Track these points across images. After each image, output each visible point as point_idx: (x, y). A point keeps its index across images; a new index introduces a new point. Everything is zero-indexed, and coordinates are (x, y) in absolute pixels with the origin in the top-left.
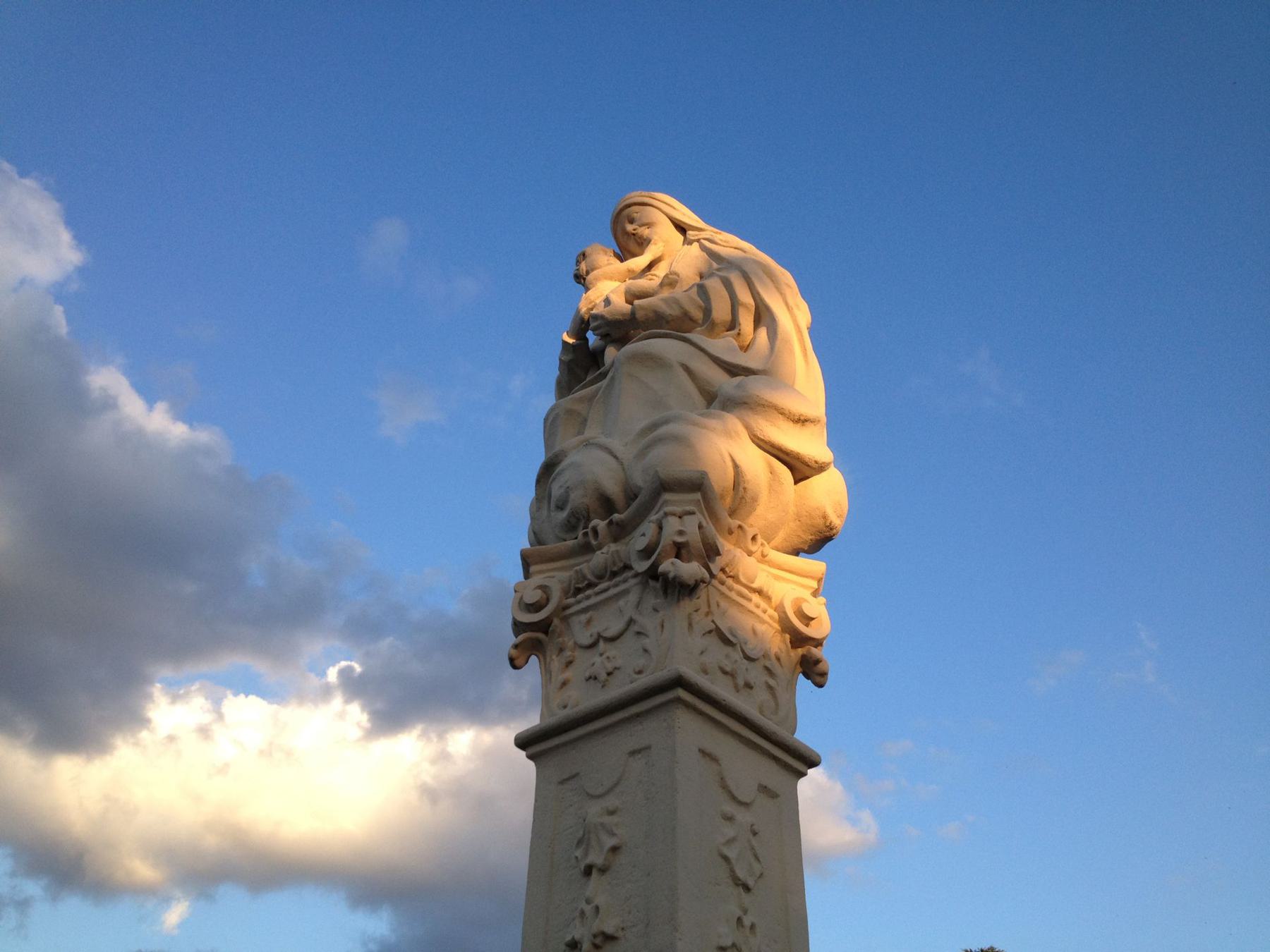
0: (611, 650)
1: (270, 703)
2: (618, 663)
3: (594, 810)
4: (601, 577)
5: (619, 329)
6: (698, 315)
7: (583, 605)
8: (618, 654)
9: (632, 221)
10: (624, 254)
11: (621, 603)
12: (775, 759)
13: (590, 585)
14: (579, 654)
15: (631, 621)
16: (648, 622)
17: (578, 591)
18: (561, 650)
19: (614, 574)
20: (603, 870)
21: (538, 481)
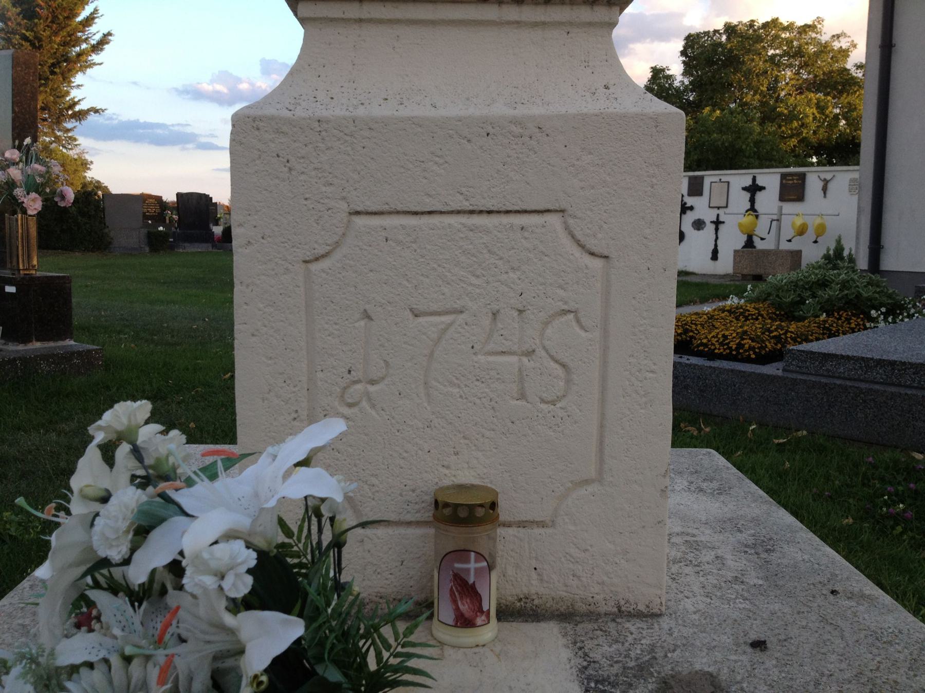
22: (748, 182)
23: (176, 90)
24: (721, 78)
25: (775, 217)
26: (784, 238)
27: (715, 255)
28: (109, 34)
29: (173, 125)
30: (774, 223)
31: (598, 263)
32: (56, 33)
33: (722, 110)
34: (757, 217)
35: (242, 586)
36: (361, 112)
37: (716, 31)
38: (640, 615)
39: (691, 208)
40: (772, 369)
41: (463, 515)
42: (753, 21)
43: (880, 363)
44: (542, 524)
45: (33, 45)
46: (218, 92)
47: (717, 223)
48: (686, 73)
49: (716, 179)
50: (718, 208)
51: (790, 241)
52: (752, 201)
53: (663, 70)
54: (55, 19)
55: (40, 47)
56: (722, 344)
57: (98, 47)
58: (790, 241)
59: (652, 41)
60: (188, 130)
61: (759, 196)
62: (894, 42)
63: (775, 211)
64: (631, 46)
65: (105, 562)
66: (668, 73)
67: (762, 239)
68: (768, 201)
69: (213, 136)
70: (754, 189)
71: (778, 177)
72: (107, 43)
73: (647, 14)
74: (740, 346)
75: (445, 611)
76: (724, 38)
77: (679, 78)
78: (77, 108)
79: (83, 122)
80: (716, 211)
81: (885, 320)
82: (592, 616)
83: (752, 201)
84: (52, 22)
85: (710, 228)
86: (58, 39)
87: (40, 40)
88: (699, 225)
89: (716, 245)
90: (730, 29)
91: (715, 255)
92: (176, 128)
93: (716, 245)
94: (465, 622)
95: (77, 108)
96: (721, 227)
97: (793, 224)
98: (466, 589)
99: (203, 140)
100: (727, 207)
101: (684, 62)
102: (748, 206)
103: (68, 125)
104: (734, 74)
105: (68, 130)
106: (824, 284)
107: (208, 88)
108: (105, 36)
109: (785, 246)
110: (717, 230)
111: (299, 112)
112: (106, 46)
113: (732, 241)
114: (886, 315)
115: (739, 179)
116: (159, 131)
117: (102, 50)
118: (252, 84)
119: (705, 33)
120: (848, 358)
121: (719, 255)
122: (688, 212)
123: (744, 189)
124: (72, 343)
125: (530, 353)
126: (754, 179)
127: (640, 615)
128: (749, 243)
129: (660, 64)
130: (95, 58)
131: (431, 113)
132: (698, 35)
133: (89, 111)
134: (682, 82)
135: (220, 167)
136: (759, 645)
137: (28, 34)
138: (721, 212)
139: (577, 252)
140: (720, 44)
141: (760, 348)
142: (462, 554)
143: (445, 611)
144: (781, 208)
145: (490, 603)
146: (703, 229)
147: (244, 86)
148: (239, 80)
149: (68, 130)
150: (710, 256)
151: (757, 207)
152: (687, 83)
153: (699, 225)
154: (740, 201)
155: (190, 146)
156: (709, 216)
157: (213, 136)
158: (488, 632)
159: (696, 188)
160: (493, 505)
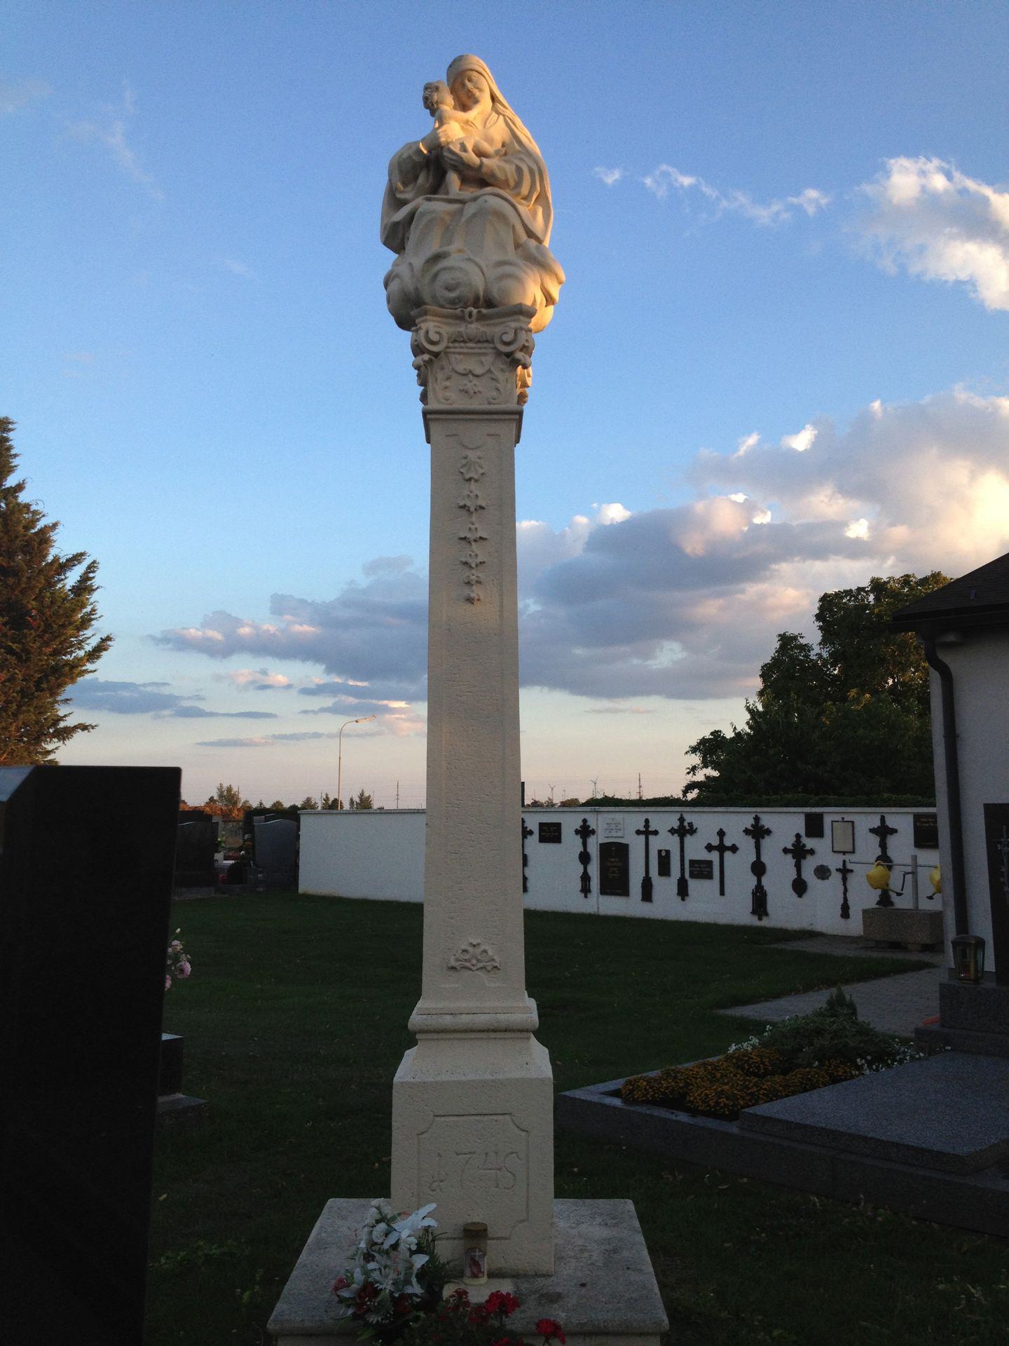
0: (475, 381)
1: (936, 576)
2: (480, 389)
3: (472, 455)
4: (471, 340)
5: (45, 631)
6: (512, 183)
7: (466, 351)
8: (478, 385)
9: (470, 80)
10: (464, 107)
11: (483, 359)
12: (467, 420)
13: (464, 342)
14: (454, 375)
15: (489, 371)
16: (499, 375)
17: (455, 341)
18: (442, 368)
19: (479, 342)
20: (476, 481)
21: (427, 262)
22: (876, 823)
23: (153, 638)
24: (870, 650)
25: (909, 869)
26: (923, 895)
27: (845, 912)
28: (108, 639)
29: (144, 685)
30: (909, 877)
31: (523, 1134)
32: (47, 644)
33: (874, 692)
34: (890, 868)
35: (414, 1248)
36: (438, 1079)
37: (860, 589)
38: (544, 1276)
39: (812, 852)
40: (733, 1128)
41: (475, 1235)
42: (908, 576)
43: (798, 1126)
44: (506, 1239)
45: (19, 658)
46: (210, 640)
47: (845, 872)
48: (823, 642)
49: (838, 818)
50: (844, 853)
51: (931, 898)
52: (883, 846)
53: (795, 638)
54: (48, 626)
55: (28, 659)
56: (704, 1102)
57: (95, 654)
58: (931, 898)
59: (804, 560)
60: (166, 691)
61: (892, 841)
62: (958, 732)
63: (909, 861)
64: (774, 567)
65: (376, 1244)
66: (803, 641)
67: (899, 894)
68: (902, 846)
69: (199, 698)
70: (883, 832)
71: (910, 819)
72: (105, 650)
73: (794, 523)
74: (717, 1103)
75: (468, 1272)
76: (871, 597)
77: (817, 649)
78: (62, 725)
79: (67, 742)
80: (841, 857)
81: (870, 1067)
82: (525, 1276)
83: (883, 846)
84: (45, 631)
85: (836, 878)
86: (48, 650)
87: (28, 652)
88: (822, 872)
89: (845, 899)
90: (878, 586)
91: (845, 912)
92: (149, 689)
93: (845, 899)
94: (475, 1276)
95: (62, 725)
96: (849, 876)
97: (931, 879)
98: (476, 1264)
99: (185, 704)
100: (853, 852)
101: (821, 628)
102: (879, 852)
103: (49, 747)
104: (887, 645)
105: (49, 752)
106: (819, 1032)
107: (194, 632)
108: (103, 640)
109: (925, 905)
110: (845, 880)
111: (417, 1080)
112: (104, 653)
113: (864, 897)
114: (870, 1064)
115: (866, 819)
116: (125, 694)
117: (98, 657)
118: (256, 627)
119: (845, 591)
120: (779, 1121)
121: (851, 912)
122: (809, 857)
123: (872, 831)
124: (181, 1096)
125: (500, 1169)
126: (883, 819)
127: (544, 1276)
128: (885, 900)
129: (792, 630)
130: (89, 666)
131: (463, 1078)
132: (837, 595)
133: (76, 727)
134: (820, 656)
135: (207, 740)
136: (583, 1285)
137: (14, 646)
138: (847, 857)
139: (516, 1130)
140: (867, 606)
141: (734, 1105)
142: (473, 1249)
143: (468, 1272)
144: (915, 858)
145: (485, 1268)
146: (827, 878)
147: (245, 631)
148: (238, 622)
149: (49, 752)
150: (840, 912)
151: (890, 853)
152: (825, 655)
153: (822, 872)
154: (868, 847)
155: (167, 712)
156: (834, 862)
157: (199, 698)
158: (484, 1280)
159: (815, 827)
160: (486, 1230)
